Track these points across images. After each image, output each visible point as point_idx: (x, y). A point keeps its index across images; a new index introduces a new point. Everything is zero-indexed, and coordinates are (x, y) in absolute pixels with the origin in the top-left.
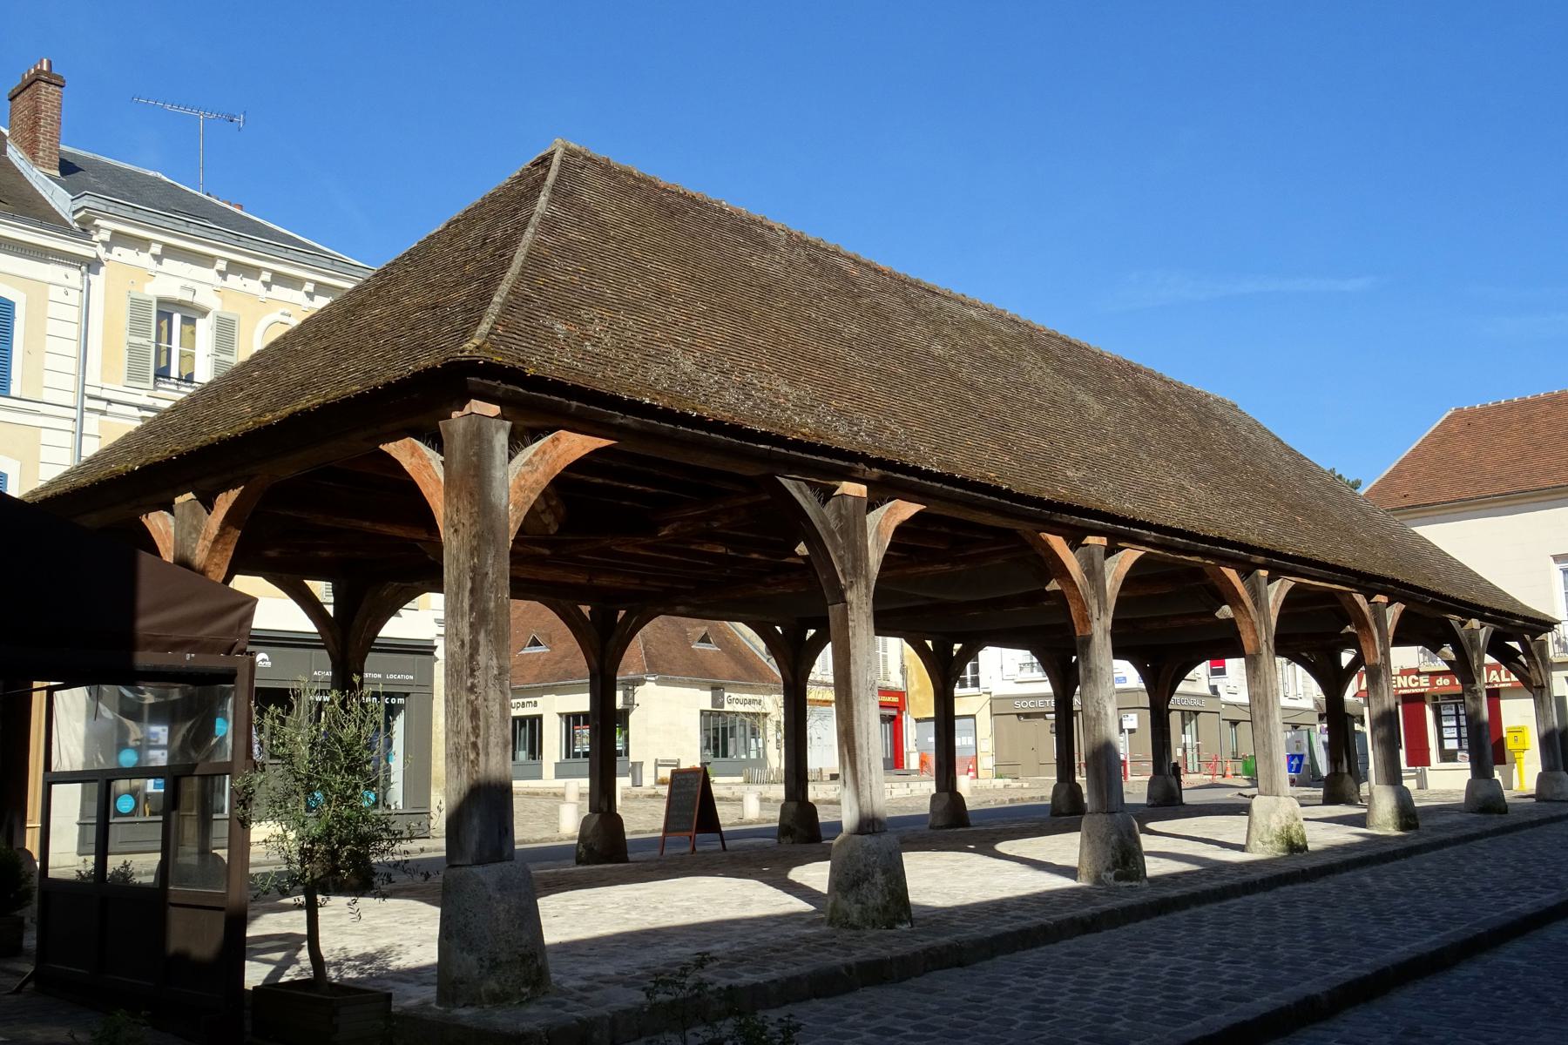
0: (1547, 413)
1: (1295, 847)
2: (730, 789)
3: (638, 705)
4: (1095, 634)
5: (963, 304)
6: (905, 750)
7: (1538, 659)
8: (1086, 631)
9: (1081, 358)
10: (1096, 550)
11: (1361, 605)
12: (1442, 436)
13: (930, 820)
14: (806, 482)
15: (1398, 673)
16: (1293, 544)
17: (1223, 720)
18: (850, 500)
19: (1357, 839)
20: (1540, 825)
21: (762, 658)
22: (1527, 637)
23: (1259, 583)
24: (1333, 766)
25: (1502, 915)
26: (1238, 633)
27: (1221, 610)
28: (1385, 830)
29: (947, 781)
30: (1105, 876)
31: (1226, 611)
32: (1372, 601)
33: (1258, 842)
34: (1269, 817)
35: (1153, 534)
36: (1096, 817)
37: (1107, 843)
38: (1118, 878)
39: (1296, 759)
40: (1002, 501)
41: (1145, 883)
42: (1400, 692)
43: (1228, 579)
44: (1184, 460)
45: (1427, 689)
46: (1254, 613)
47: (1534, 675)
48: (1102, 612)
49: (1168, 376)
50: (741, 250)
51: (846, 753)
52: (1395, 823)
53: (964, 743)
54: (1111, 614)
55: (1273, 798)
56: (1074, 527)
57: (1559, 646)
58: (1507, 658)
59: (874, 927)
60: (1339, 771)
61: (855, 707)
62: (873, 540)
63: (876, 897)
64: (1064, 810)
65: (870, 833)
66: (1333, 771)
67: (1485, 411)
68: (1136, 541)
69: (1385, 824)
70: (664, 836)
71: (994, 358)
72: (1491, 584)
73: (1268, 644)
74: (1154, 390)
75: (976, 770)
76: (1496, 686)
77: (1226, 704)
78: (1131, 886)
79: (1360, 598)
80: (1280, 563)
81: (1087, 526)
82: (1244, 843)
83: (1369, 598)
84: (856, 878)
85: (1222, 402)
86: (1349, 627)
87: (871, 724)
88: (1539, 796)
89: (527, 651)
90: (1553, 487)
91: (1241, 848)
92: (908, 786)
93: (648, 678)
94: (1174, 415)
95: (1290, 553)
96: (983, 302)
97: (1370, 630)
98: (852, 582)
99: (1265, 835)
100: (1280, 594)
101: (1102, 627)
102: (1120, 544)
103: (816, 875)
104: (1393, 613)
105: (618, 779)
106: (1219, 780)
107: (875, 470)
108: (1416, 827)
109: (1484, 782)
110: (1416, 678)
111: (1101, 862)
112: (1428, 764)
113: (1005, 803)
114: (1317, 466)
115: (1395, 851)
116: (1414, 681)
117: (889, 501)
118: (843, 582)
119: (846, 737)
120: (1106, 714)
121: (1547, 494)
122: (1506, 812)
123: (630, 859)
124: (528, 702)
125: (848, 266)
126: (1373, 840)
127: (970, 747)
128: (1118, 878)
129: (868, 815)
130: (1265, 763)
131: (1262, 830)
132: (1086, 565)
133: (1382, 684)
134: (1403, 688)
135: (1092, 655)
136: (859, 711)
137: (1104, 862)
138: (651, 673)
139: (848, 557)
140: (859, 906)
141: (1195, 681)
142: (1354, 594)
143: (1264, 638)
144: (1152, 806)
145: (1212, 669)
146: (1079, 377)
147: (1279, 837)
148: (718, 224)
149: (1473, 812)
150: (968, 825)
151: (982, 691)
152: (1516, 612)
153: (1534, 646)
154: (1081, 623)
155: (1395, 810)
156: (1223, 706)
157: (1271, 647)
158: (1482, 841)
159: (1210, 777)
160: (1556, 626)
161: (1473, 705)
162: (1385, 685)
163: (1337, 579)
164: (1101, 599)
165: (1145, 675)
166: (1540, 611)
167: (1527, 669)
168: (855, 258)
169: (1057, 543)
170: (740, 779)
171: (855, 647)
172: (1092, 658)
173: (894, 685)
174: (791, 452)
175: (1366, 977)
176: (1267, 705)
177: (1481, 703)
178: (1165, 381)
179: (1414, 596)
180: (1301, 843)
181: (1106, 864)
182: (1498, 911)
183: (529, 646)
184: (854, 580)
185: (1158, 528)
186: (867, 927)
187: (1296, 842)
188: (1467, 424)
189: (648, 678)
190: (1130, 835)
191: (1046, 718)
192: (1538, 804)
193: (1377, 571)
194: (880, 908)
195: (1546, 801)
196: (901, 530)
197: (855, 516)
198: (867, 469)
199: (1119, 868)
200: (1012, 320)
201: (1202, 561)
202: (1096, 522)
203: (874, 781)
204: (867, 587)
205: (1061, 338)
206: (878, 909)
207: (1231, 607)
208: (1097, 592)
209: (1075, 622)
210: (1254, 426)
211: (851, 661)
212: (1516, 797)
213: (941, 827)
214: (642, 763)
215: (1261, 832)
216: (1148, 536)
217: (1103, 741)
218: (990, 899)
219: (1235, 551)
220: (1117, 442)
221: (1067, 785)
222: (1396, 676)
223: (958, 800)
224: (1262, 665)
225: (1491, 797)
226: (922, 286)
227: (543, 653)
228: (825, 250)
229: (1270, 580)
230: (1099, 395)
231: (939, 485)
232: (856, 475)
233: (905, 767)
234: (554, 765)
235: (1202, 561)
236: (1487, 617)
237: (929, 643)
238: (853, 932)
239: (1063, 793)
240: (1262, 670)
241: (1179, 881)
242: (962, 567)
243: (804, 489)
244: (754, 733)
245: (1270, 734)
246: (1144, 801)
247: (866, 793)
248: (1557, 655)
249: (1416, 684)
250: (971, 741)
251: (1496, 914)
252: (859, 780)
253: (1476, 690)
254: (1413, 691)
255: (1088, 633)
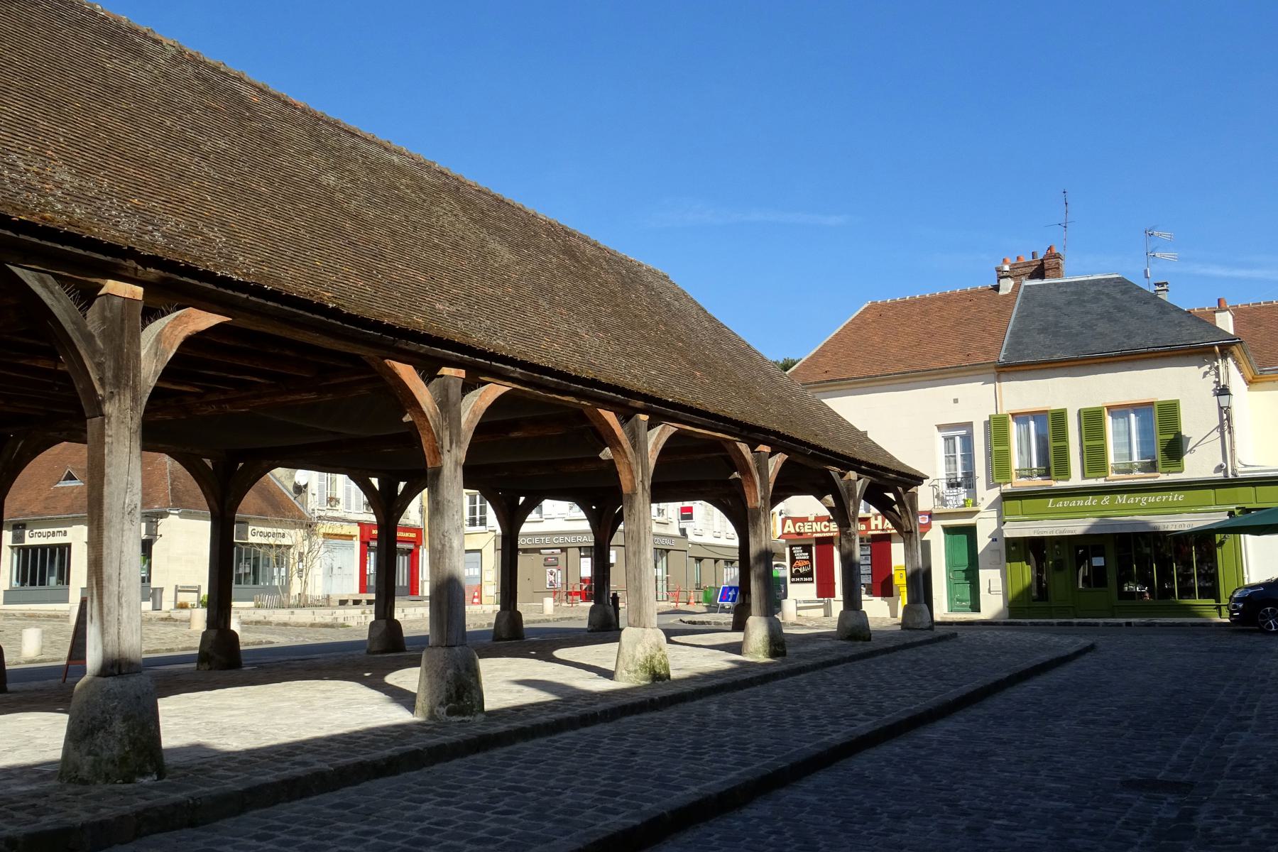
0: (941, 309)
1: (658, 677)
2: (238, 613)
3: (161, 536)
4: (444, 467)
5: (386, 149)
6: (420, 579)
7: (909, 508)
8: (436, 462)
9: (509, 214)
10: (452, 381)
11: (744, 453)
12: (859, 325)
13: (368, 646)
14: (56, 277)
15: (813, 519)
16: (675, 393)
17: (690, 557)
18: (116, 301)
19: (727, 666)
20: (894, 651)
21: (290, 496)
22: (900, 489)
23: (638, 428)
24: (742, 598)
25: (811, 747)
26: (617, 474)
27: (604, 451)
28: (756, 658)
29: (385, 607)
30: (438, 711)
31: (606, 454)
32: (756, 450)
33: (624, 671)
34: (634, 647)
35: (518, 370)
36: (435, 651)
37: (443, 678)
38: (450, 713)
39: (733, 590)
40: (330, 320)
41: (480, 717)
42: (815, 535)
43: (605, 420)
44: (590, 312)
45: (835, 534)
46: (631, 454)
47: (905, 522)
48: (454, 445)
49: (603, 243)
50: (98, 50)
51: (94, 585)
52: (765, 651)
53: (472, 574)
54: (466, 446)
55: (640, 629)
56: (425, 357)
57: (938, 500)
58: (885, 508)
59: (107, 782)
60: (747, 602)
61: (105, 533)
62: (150, 348)
63: (112, 746)
64: (504, 636)
65: (115, 675)
66: (742, 602)
67: (894, 305)
68: (501, 376)
69: (757, 652)
70: (68, 664)
71: (401, 199)
72: (874, 443)
73: (643, 485)
74: (584, 253)
75: (480, 597)
76: (889, 532)
77: (692, 544)
78: (463, 721)
79: (744, 448)
80: (660, 410)
81: (440, 355)
82: (614, 670)
83: (753, 449)
84: (90, 726)
85: (655, 273)
86: (736, 473)
87: (125, 553)
88: (904, 625)
89: (62, 484)
90: (940, 369)
91: (609, 675)
92: (403, 611)
93: (171, 512)
94: (597, 275)
95: (670, 400)
96: (410, 151)
97: (752, 476)
98: (112, 393)
99: (630, 665)
100: (660, 439)
101: (453, 459)
102: (482, 378)
103: (408, 678)
104: (775, 463)
105: (980, 570)
106: (682, 606)
107: (153, 270)
108: (784, 654)
109: (853, 613)
110: (827, 524)
111: (435, 696)
112: (834, 597)
113: (483, 626)
114: (735, 334)
115: (751, 678)
116: (825, 527)
117: (179, 308)
118: (100, 392)
119: (96, 567)
120: (451, 547)
121: (934, 375)
122: (869, 639)
123: (407, 650)
124: (58, 532)
125: (245, 91)
126: (702, 676)
127: (476, 577)
128: (450, 713)
129: (113, 654)
130: (635, 596)
131: (628, 659)
132: (440, 396)
133: (760, 525)
134: (817, 532)
135: (441, 487)
136: (110, 538)
137: (438, 697)
138: (175, 507)
139: (109, 364)
140: (91, 758)
141: (668, 524)
142: (737, 443)
143: (640, 479)
144: (592, 631)
145: (682, 515)
146: (499, 229)
147: (643, 667)
148: (81, 24)
149: (842, 639)
150: (403, 650)
151: (488, 529)
152: (891, 467)
153: (906, 497)
154: (432, 454)
155: (766, 639)
156: (690, 546)
157: (647, 487)
158: (837, 667)
159: (675, 604)
160: (924, 481)
161: (847, 546)
162: (763, 526)
163: (719, 427)
164: (455, 431)
165: (591, 517)
166: (913, 467)
167: (900, 517)
168: (262, 87)
169: (406, 372)
170: (252, 604)
171: (111, 465)
172: (441, 491)
173: (412, 523)
174: (21, 236)
175: (635, 828)
176: (639, 542)
177: (854, 545)
178: (599, 248)
179: (796, 447)
180: (663, 672)
181: (440, 698)
182: (810, 742)
183: (64, 480)
184: (115, 391)
185: (523, 365)
186: (98, 782)
187: (658, 671)
188: (879, 316)
189: (171, 512)
190: (467, 669)
191: (541, 554)
192: (902, 631)
193: (761, 423)
194: (116, 759)
195: (909, 629)
196: (192, 342)
197: (123, 320)
198: (139, 267)
199: (452, 702)
200: (441, 172)
201: (576, 401)
202: (451, 352)
203: (125, 616)
204: (135, 399)
205: (493, 196)
206: (113, 761)
207: (610, 448)
208: (450, 424)
209: (426, 454)
210: (681, 295)
211: (105, 482)
212: (895, 624)
213: (377, 652)
214: (162, 589)
215: (627, 661)
216: (513, 372)
217: (447, 574)
218: (370, 725)
219: (611, 394)
220: (517, 287)
221: (508, 613)
222: (812, 522)
223: (395, 627)
224: (637, 504)
225: (857, 626)
226: (341, 126)
227: (77, 486)
228: (225, 73)
229: (651, 426)
230: (515, 247)
231: (245, 296)
232: (127, 274)
233: (420, 594)
234: (3, 592)
235: (576, 401)
236: (863, 469)
237: (375, 481)
238: (80, 788)
239: (504, 620)
240: (637, 509)
241: (521, 713)
242: (329, 397)
243: (50, 284)
244: (279, 563)
245: (640, 570)
246: (585, 625)
247: (113, 630)
248: (936, 507)
249: (827, 529)
250: (477, 572)
251: (807, 745)
252: (105, 615)
253: (850, 533)
254: (824, 535)
255: (438, 465)
